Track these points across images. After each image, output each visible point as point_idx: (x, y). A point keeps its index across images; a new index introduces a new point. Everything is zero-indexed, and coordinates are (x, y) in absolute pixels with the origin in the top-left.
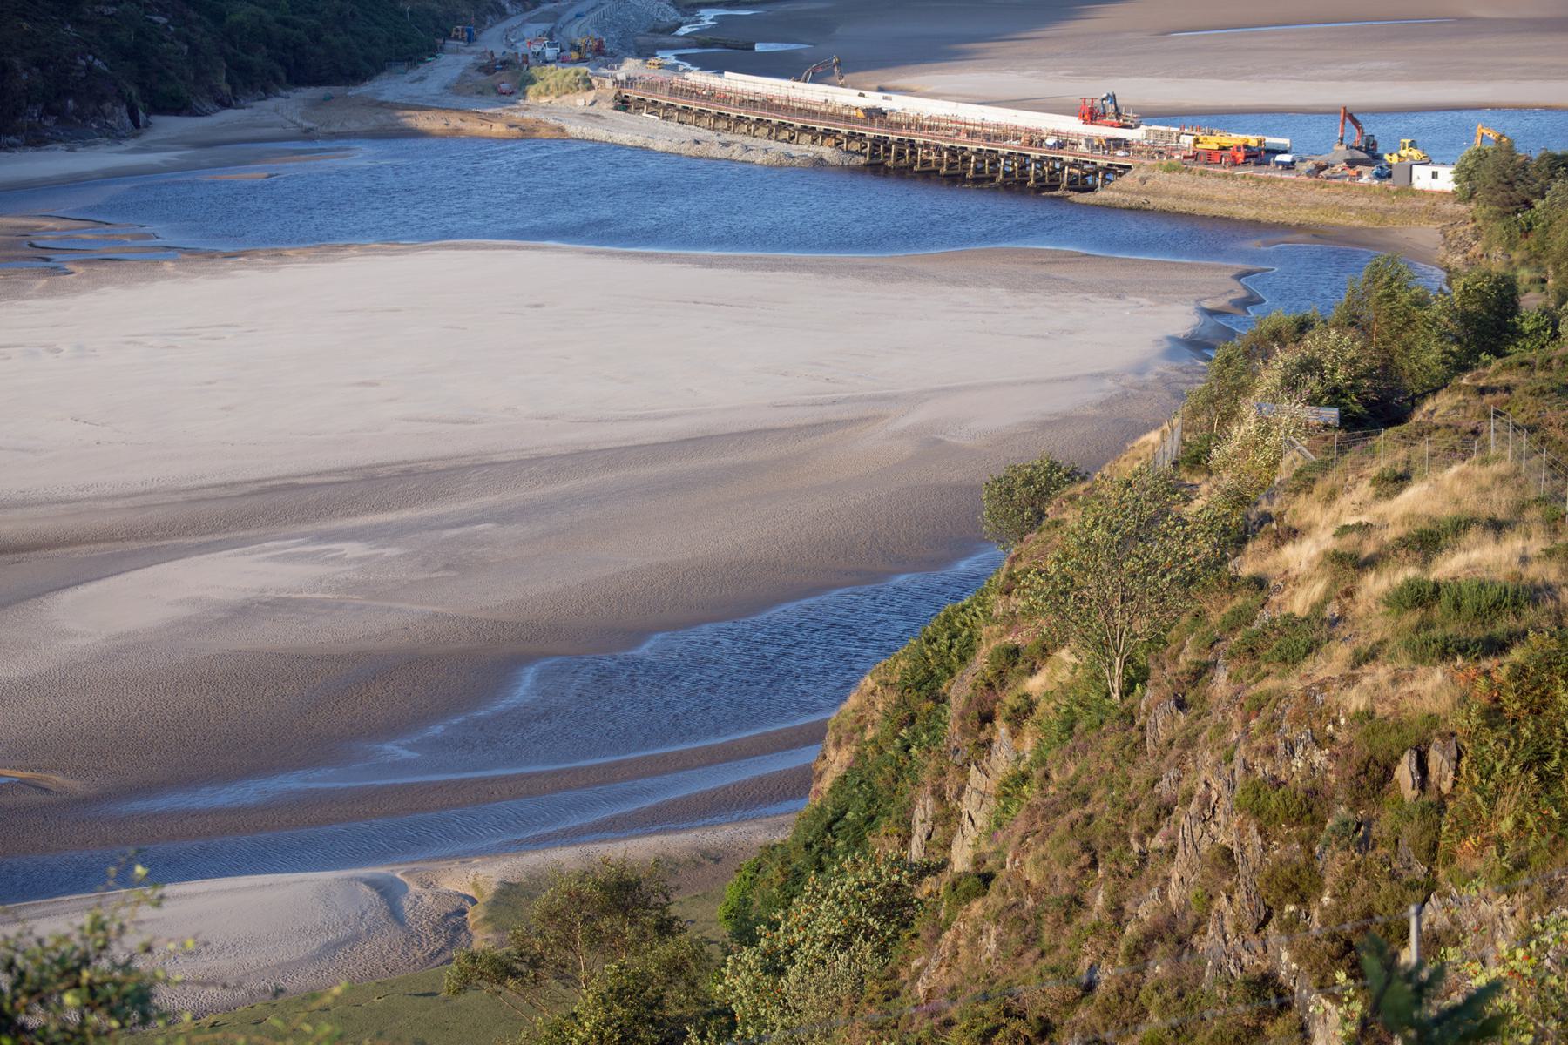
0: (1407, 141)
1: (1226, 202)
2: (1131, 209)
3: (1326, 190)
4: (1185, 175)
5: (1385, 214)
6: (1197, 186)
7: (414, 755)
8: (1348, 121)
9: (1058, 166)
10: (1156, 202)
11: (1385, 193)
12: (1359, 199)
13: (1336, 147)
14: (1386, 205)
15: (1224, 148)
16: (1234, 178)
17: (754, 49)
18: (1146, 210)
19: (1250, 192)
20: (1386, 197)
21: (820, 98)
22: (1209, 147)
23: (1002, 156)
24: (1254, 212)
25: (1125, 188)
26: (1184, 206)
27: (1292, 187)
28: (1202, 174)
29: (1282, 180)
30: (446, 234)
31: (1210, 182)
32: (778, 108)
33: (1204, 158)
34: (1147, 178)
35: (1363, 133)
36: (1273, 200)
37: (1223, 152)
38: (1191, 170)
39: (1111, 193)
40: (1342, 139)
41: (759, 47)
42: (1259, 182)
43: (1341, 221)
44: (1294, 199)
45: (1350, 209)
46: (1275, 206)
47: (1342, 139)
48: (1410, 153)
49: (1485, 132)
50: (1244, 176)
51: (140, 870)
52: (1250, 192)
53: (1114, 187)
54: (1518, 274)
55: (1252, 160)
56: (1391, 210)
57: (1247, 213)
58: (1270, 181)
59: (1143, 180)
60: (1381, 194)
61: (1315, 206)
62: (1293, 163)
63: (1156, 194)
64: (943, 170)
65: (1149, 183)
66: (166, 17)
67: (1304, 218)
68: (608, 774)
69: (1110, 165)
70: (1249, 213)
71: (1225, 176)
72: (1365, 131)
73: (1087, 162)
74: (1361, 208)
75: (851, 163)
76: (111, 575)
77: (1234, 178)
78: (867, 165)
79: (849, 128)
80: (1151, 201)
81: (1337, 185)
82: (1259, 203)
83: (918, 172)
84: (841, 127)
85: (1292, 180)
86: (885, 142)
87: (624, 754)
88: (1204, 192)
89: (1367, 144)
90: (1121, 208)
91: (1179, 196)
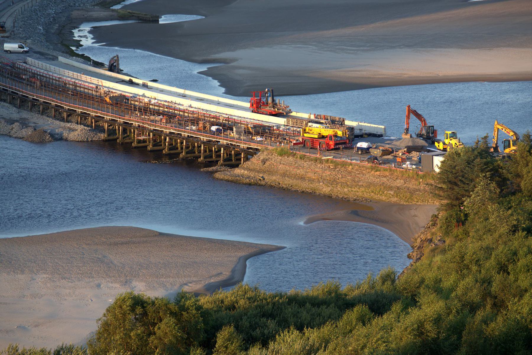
0: (449, 132)
1: (311, 181)
2: (250, 184)
3: (378, 173)
4: (291, 158)
5: (412, 192)
6: (297, 167)
8: (412, 115)
10: (270, 179)
11: (415, 176)
12: (398, 181)
13: (404, 136)
14: (414, 187)
15: (323, 137)
16: (321, 161)
17: (158, 21)
18: (260, 185)
20: (416, 180)
22: (312, 136)
24: (329, 189)
25: (251, 167)
26: (286, 182)
27: (357, 170)
28: (302, 158)
29: (351, 164)
30: (193, 91)
33: (309, 144)
34: (267, 160)
35: (425, 124)
36: (343, 180)
37: (321, 140)
38: (295, 155)
39: (243, 171)
40: (407, 130)
41: (163, 20)
42: (336, 165)
43: (383, 198)
45: (391, 188)
46: (345, 185)
47: (407, 130)
48: (451, 142)
49: (500, 128)
50: (328, 160)
53: (245, 167)
54: (206, 334)
55: (341, 147)
57: (324, 190)
58: (344, 164)
59: (264, 162)
60: (413, 177)
61: (370, 185)
62: (368, 149)
63: (271, 172)
64: (150, 147)
65: (267, 163)
67: (360, 194)
69: (248, 148)
70: (326, 190)
71: (316, 160)
72: (427, 122)
74: (398, 188)
75: (94, 139)
77: (321, 161)
78: (105, 141)
80: (266, 178)
81: (385, 170)
82: (333, 182)
83: (135, 147)
84: (90, 111)
85: (357, 165)
88: (300, 172)
89: (428, 133)
90: (243, 184)
91: (284, 175)
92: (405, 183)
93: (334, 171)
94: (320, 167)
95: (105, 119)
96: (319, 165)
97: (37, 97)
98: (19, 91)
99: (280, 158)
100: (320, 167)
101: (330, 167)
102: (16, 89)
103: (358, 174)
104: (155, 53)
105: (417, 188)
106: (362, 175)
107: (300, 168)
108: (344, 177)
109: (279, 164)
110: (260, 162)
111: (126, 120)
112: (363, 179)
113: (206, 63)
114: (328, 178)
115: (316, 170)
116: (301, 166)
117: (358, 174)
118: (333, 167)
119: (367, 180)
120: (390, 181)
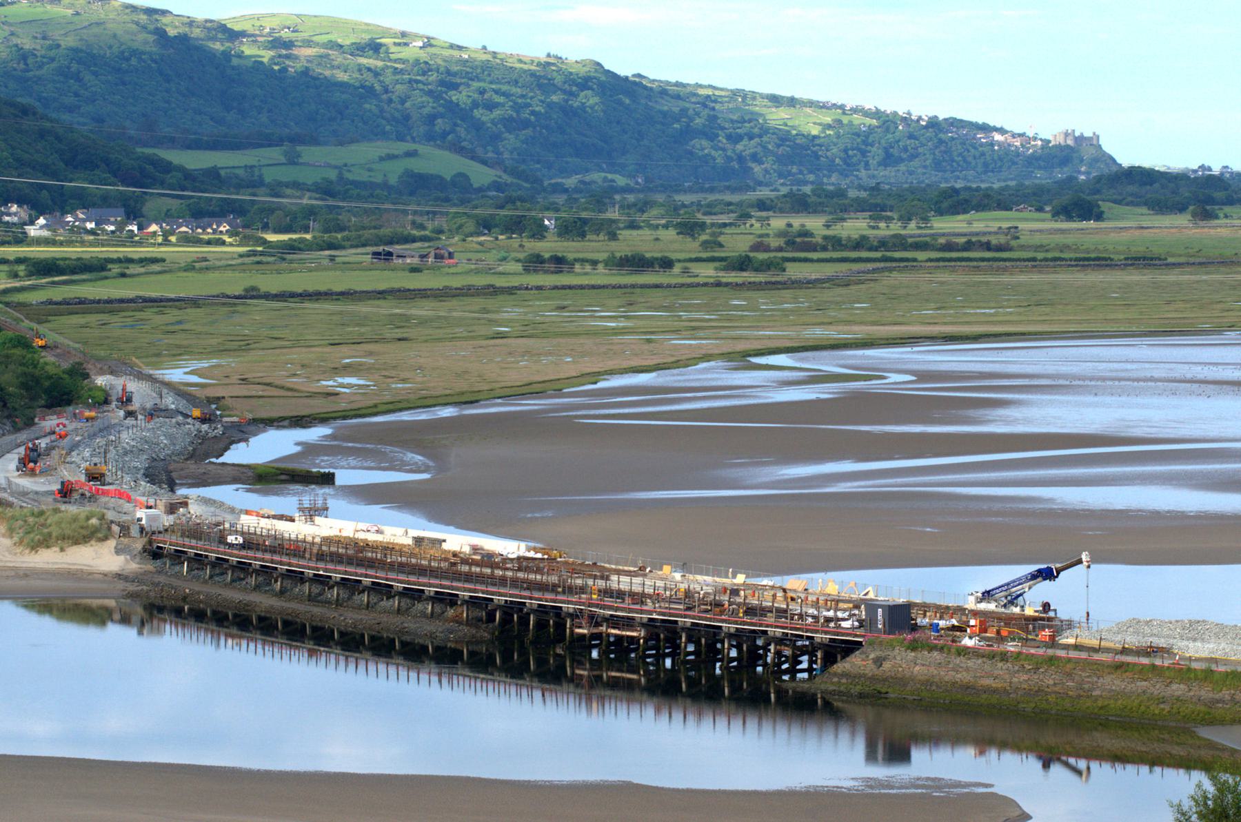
7: (539, 556)
9: (760, 642)
12: (1174, 686)
14: (1211, 695)
19: (1025, 677)
21: (856, 256)
23: (683, 629)
29: (1070, 660)
31: (970, 664)
32: (371, 563)
44: (1086, 686)
51: (996, 148)
52: (1025, 677)
56: (1218, 701)
65: (887, 665)
66: (674, 128)
68: (878, 389)
73: (801, 636)
76: (233, 465)
79: (470, 590)
86: (521, 610)
87: (623, 678)
92: (1190, 690)
93: (1035, 673)
94: (1004, 668)
95: (333, 579)
96: (1000, 665)
97: (326, 570)
98: (281, 563)
99: (913, 654)
100: (1004, 668)
101: (1024, 667)
102: (184, 546)
103: (1088, 677)
104: (944, 474)
105: (1217, 696)
106: (1095, 679)
107: (960, 670)
108: (1059, 684)
109: (913, 665)
110: (870, 662)
111: (740, 625)
112: (1099, 685)
113: (1222, 515)
114: (1026, 686)
115: (996, 672)
116: (961, 667)
117: (1088, 677)
118: (1030, 667)
119: (1109, 687)
120: (1157, 687)
